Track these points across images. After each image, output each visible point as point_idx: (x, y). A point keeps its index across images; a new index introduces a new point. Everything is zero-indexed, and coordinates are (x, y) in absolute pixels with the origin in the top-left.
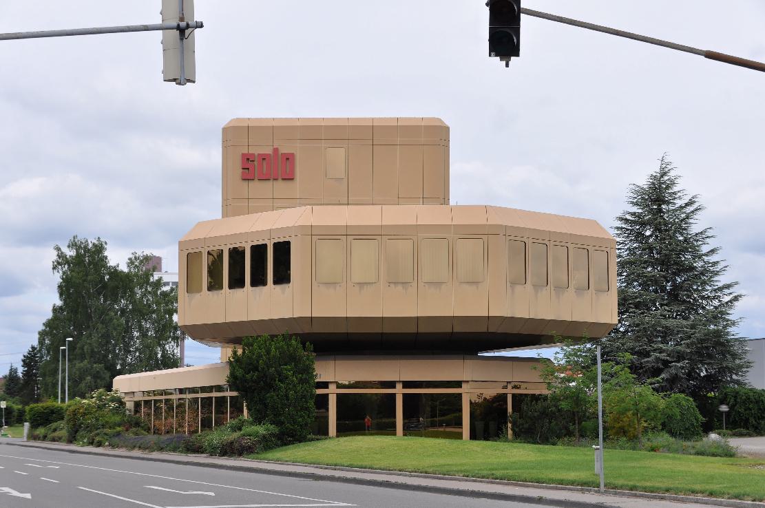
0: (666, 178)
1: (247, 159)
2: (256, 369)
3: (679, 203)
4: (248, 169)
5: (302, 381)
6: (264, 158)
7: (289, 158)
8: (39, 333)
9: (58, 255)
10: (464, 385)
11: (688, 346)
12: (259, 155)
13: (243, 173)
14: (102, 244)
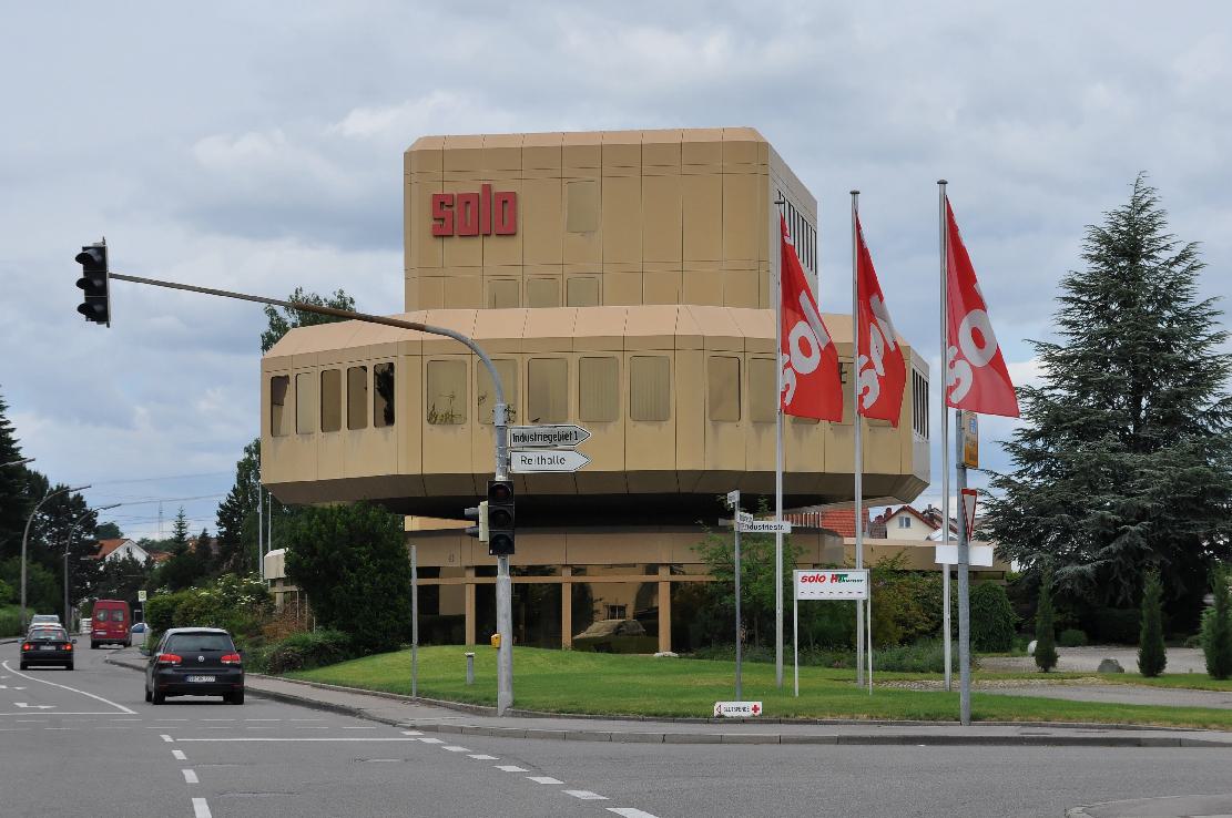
0: (1145, 214)
1: (441, 203)
2: (313, 552)
3: (1164, 256)
4: (443, 220)
5: (383, 569)
6: (467, 200)
7: (508, 200)
8: (239, 465)
9: (271, 323)
10: (661, 570)
11: (1153, 496)
12: (460, 196)
13: (434, 227)
14: (345, 304)
